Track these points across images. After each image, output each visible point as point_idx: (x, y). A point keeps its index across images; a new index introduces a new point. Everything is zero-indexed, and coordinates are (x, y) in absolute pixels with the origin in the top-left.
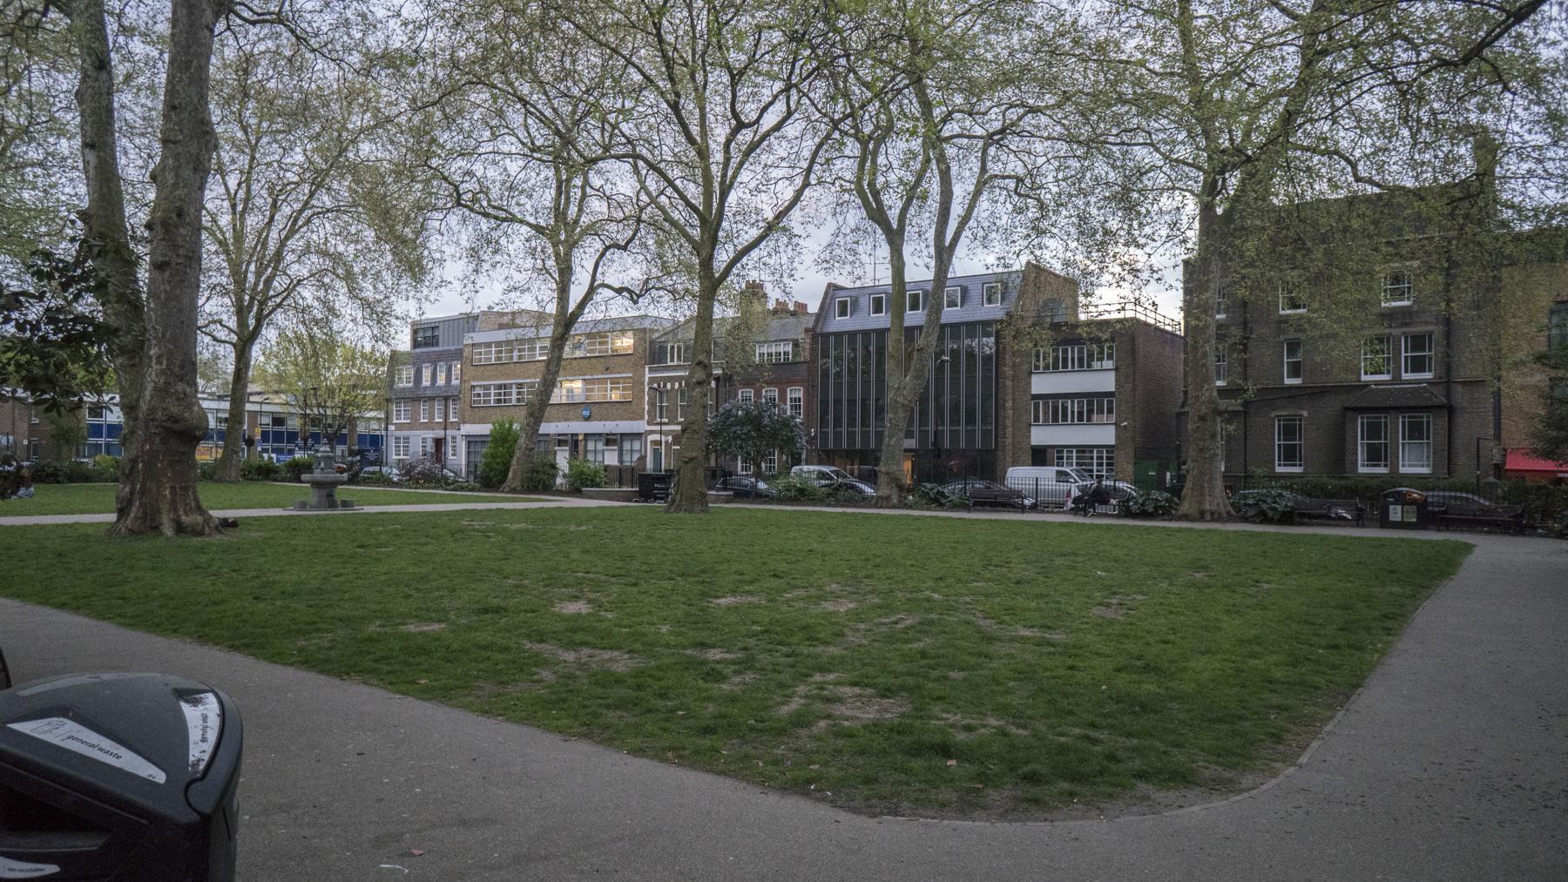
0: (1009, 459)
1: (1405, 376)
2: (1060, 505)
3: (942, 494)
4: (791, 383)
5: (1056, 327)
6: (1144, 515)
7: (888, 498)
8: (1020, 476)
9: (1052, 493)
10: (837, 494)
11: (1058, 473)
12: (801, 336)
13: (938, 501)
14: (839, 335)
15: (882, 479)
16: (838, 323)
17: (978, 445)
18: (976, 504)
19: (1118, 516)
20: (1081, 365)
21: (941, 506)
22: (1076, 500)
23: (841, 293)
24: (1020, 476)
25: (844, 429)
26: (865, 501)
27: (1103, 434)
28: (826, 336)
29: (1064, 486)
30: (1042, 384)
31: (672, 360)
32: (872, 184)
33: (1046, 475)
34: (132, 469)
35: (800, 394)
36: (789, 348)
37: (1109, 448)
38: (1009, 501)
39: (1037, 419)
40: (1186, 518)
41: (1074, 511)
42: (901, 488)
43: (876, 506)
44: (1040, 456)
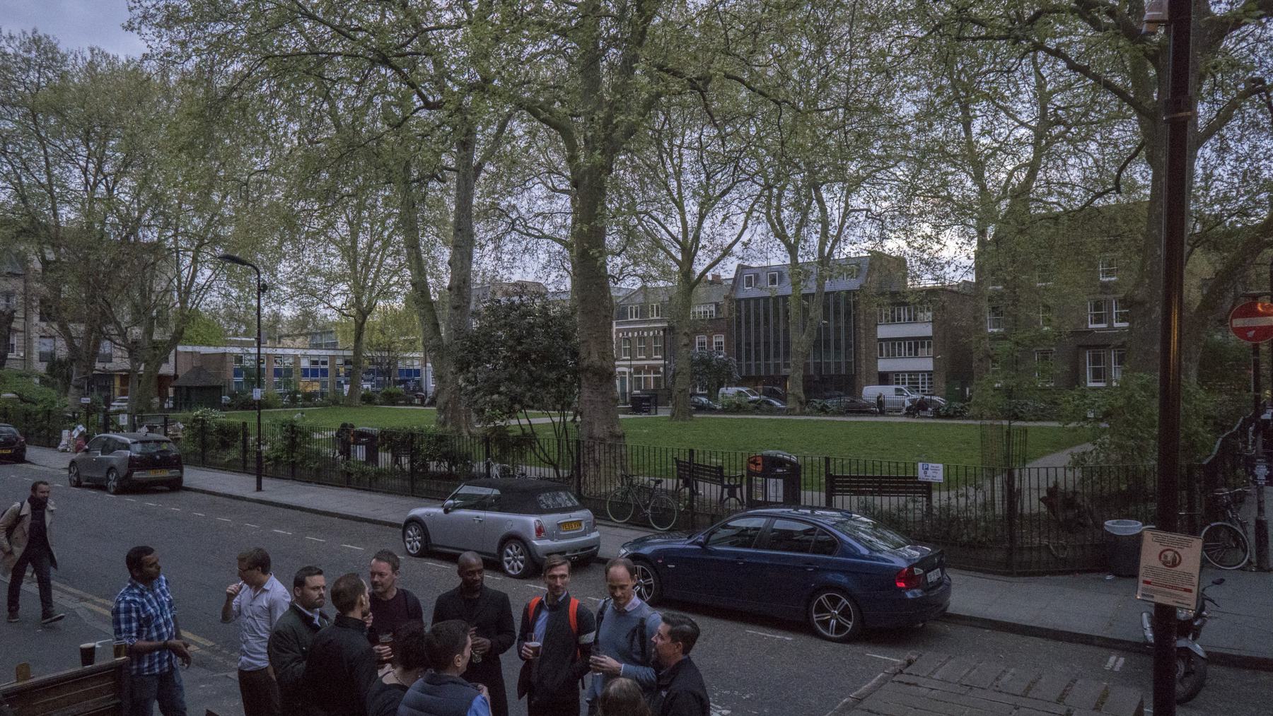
0: (864, 381)
1: (1116, 325)
2: (899, 411)
3: (827, 407)
4: (716, 332)
5: (894, 294)
6: (947, 416)
7: (794, 409)
8: (871, 392)
9: (893, 403)
10: (757, 407)
11: (897, 390)
12: (721, 300)
13: (824, 410)
14: (747, 300)
15: (790, 398)
16: (748, 292)
17: (843, 372)
18: (848, 412)
19: (933, 418)
20: (910, 354)
21: (827, 413)
22: (908, 409)
23: (747, 271)
24: (871, 392)
25: (743, 362)
26: (779, 411)
27: (926, 364)
28: (739, 301)
29: (900, 398)
30: (884, 331)
31: (632, 317)
32: (778, 218)
33: (888, 391)
34: (445, 408)
35: (722, 339)
36: (713, 308)
37: (930, 373)
38: (863, 410)
39: (881, 355)
40: (972, 417)
41: (907, 415)
42: (801, 403)
43: (786, 414)
44: (884, 378)
